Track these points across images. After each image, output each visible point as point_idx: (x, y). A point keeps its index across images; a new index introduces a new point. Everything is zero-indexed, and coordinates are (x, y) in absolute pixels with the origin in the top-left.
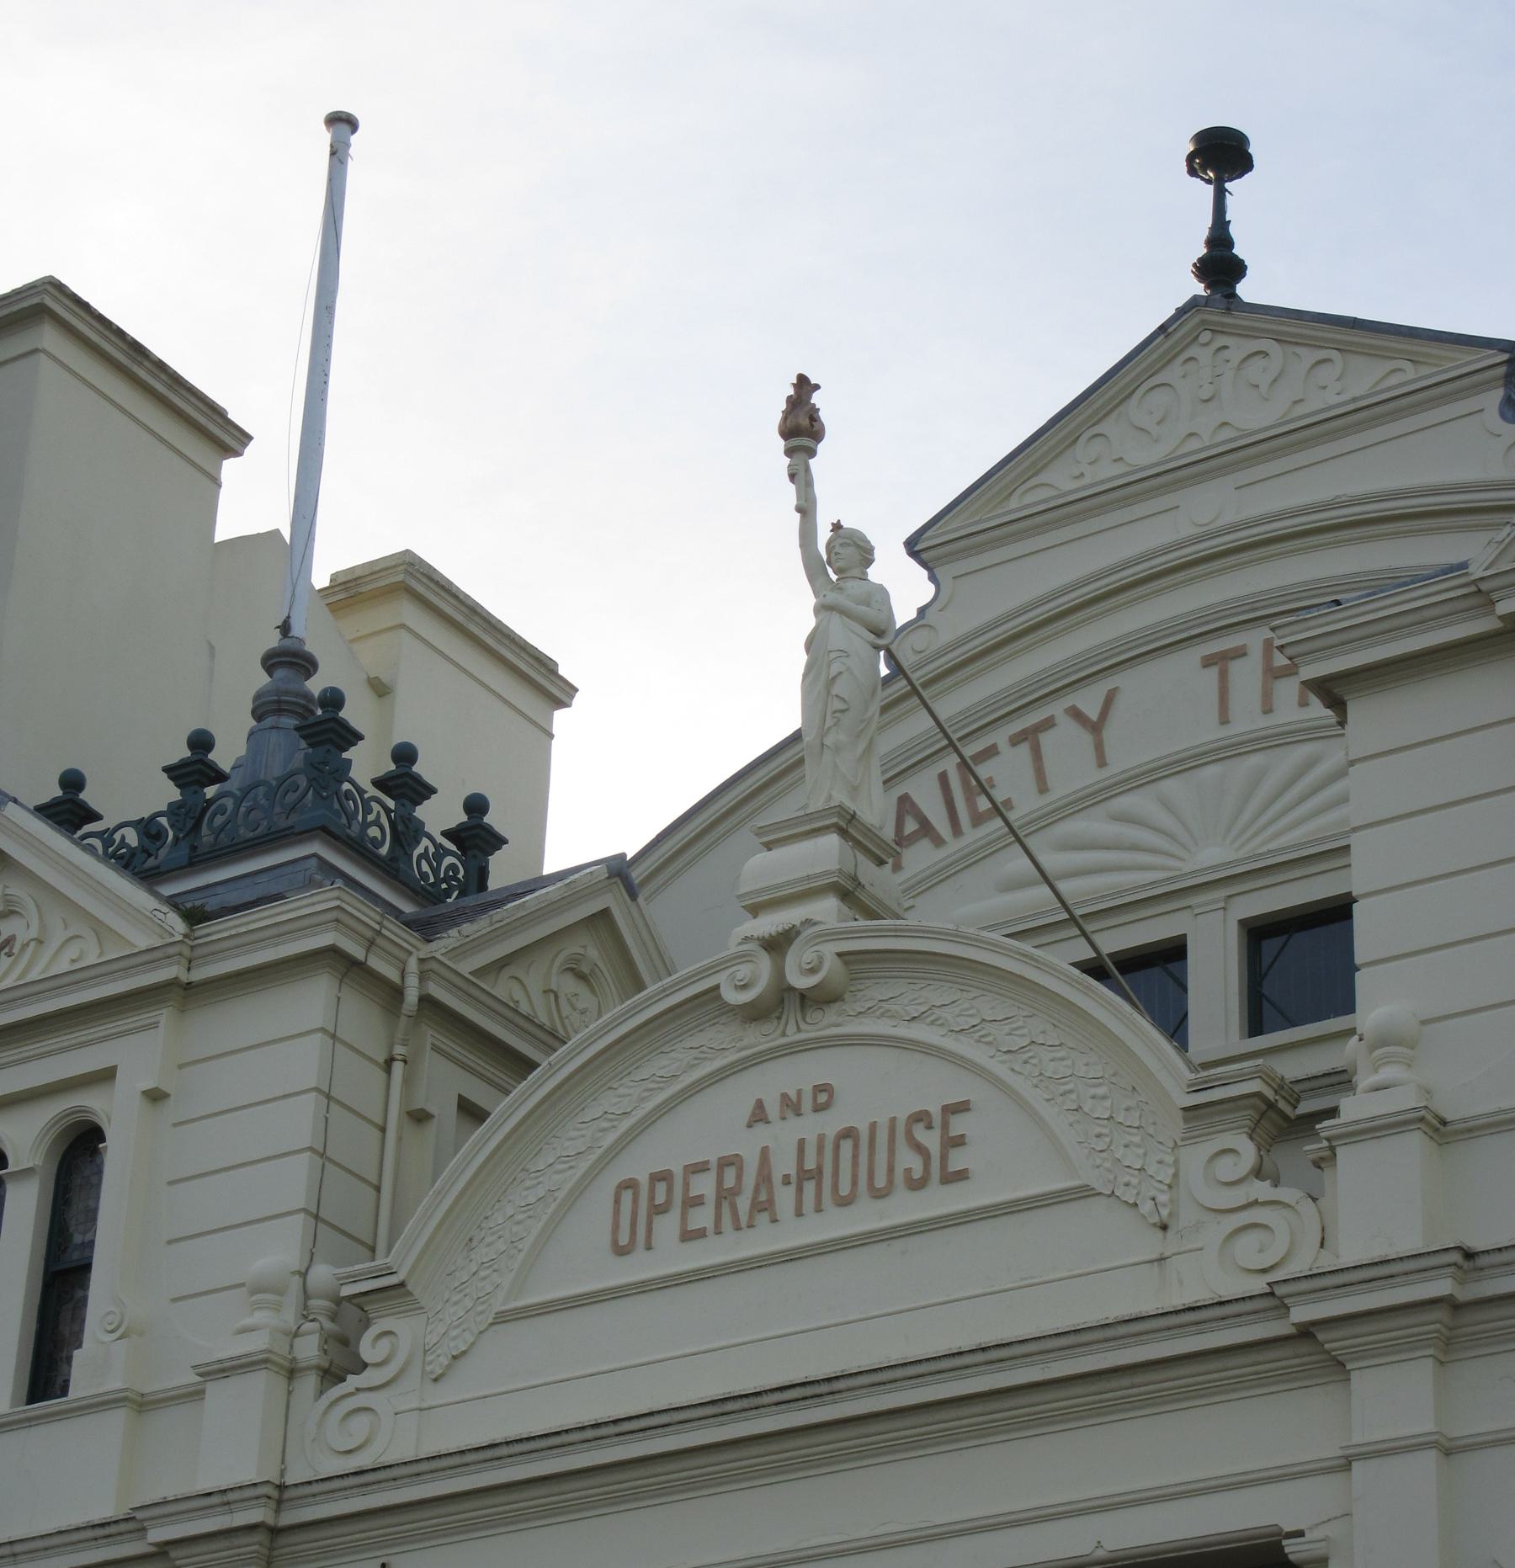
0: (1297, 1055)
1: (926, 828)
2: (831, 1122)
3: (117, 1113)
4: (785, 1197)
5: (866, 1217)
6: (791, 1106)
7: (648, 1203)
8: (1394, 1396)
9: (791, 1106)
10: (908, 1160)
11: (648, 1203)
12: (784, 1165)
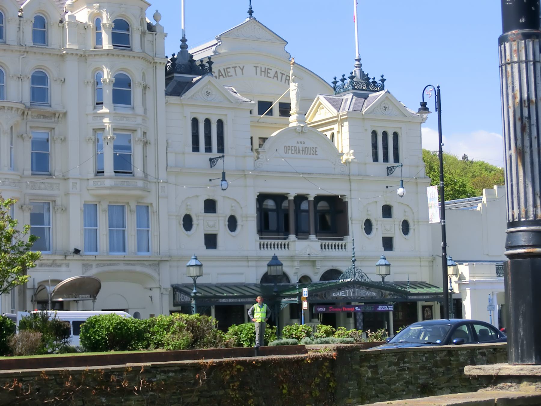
1: (222, 75)
2: (305, 146)
4: (301, 152)
5: (308, 156)
6: (301, 143)
9: (301, 143)
10: (312, 152)
12: (301, 149)
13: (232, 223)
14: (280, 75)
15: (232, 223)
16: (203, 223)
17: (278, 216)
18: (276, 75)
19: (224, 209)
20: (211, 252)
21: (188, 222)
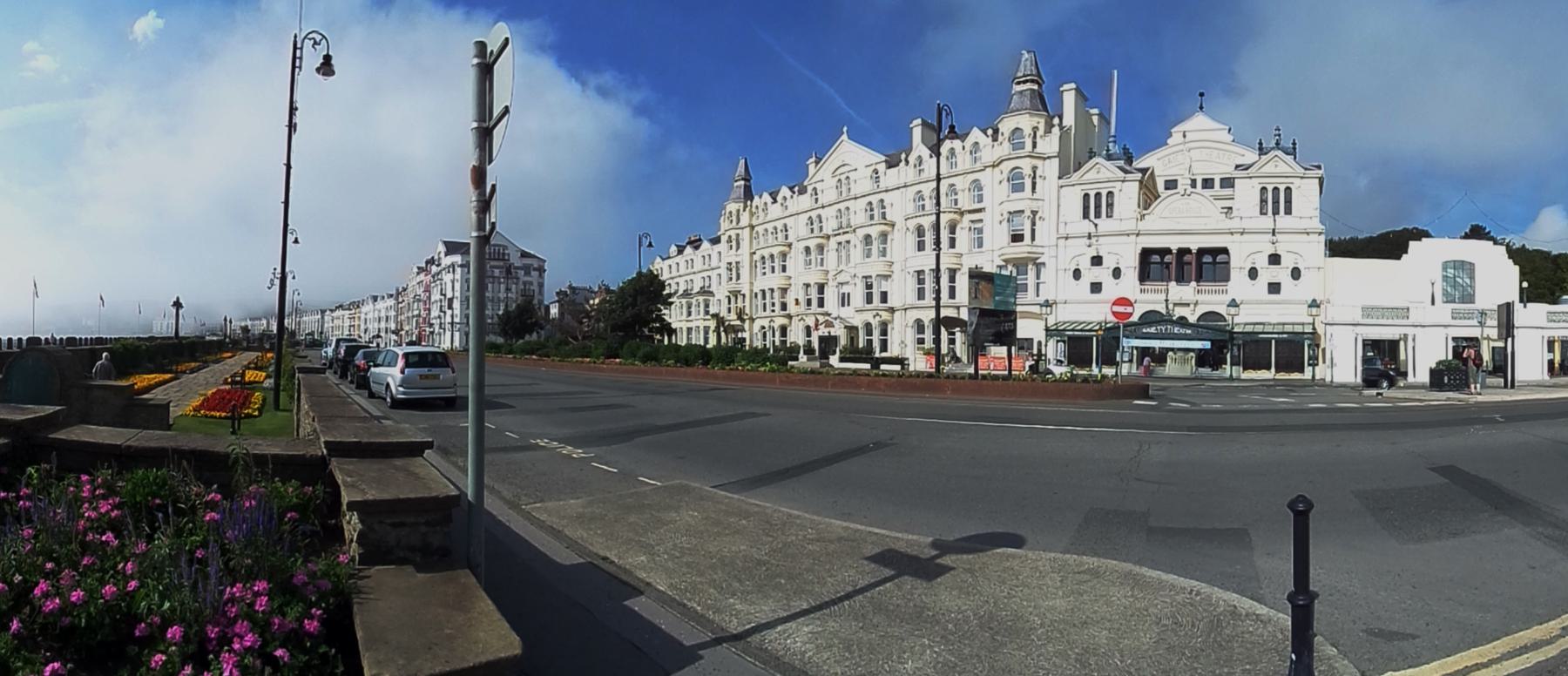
0: (1228, 192)
3: (1116, 191)
13: (1117, 273)
15: (1117, 273)
16: (1091, 274)
17: (1153, 264)
19: (1109, 263)
20: (1096, 296)
21: (1077, 274)
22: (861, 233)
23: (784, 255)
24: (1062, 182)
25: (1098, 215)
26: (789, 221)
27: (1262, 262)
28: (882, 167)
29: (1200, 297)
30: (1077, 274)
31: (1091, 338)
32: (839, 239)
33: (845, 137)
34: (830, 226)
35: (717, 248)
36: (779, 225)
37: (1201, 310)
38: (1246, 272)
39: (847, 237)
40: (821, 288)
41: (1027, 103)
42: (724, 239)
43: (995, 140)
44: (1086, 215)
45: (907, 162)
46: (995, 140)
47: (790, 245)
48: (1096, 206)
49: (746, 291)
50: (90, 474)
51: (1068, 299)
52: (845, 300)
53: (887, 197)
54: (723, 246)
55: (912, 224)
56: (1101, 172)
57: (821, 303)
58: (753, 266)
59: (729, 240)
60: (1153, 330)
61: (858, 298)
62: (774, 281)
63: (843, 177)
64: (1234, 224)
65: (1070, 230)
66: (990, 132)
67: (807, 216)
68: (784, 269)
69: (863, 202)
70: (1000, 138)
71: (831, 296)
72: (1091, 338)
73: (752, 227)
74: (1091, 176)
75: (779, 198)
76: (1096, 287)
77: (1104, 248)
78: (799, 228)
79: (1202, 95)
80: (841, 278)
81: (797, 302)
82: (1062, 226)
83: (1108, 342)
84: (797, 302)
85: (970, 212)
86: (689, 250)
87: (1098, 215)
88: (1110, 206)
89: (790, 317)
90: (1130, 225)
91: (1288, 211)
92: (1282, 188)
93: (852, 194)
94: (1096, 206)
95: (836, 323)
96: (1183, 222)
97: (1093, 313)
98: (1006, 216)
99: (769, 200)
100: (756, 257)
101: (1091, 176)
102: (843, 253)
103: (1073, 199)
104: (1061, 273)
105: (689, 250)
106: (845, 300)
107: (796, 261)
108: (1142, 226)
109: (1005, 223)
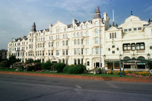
7: (129, 36)
8: (146, 40)
11: (129, 36)
14: (138, 23)
15: (118, 49)
18: (137, 23)
21: (109, 49)
22: (62, 40)
23: (44, 44)
24: (106, 31)
25: (113, 37)
26: (45, 37)
27: (111, 47)
28: (67, 27)
29: (138, 53)
30: (109, 49)
31: (113, 63)
32: (57, 41)
33: (58, 21)
34: (54, 38)
35: (27, 41)
36: (43, 37)
37: (138, 56)
38: (149, 47)
39: (58, 41)
40: (52, 51)
41: (98, 16)
42: (29, 39)
43: (92, 23)
44: (111, 38)
45: (72, 27)
46: (92, 23)
47: (45, 42)
48: (113, 36)
49: (34, 51)
50: (149, 67)
51: (108, 54)
52: (58, 54)
53: (68, 34)
54: (28, 41)
55: (73, 39)
56: (113, 29)
57: (52, 54)
58: (36, 45)
59: (30, 39)
60: (131, 61)
61: (61, 53)
62: (41, 49)
63: (58, 29)
64: (146, 37)
65: (108, 41)
66: (90, 22)
67: (49, 36)
68: (44, 47)
69: (62, 34)
70: (93, 23)
71: (55, 53)
72: (113, 63)
73: (36, 37)
74: (111, 30)
75: (43, 32)
76: (113, 52)
77: (116, 44)
78: (47, 39)
79: (132, 12)
80: (57, 49)
81: (47, 54)
82: (106, 40)
83: (117, 64)
84: (47, 54)
85: (86, 37)
86: (19, 41)
87: (113, 37)
88: (115, 35)
89: (45, 57)
90: (121, 39)
91: (115, 37)
92: (114, 33)
93: (60, 32)
94: (113, 36)
95: (56, 59)
96: (130, 38)
97: (116, 57)
98: (94, 38)
99: (41, 32)
100: (37, 44)
101: (111, 30)
102: (58, 44)
103: (108, 34)
104: (106, 49)
105: (19, 41)
106: (58, 54)
107: (47, 45)
108: (123, 39)
109: (94, 40)
